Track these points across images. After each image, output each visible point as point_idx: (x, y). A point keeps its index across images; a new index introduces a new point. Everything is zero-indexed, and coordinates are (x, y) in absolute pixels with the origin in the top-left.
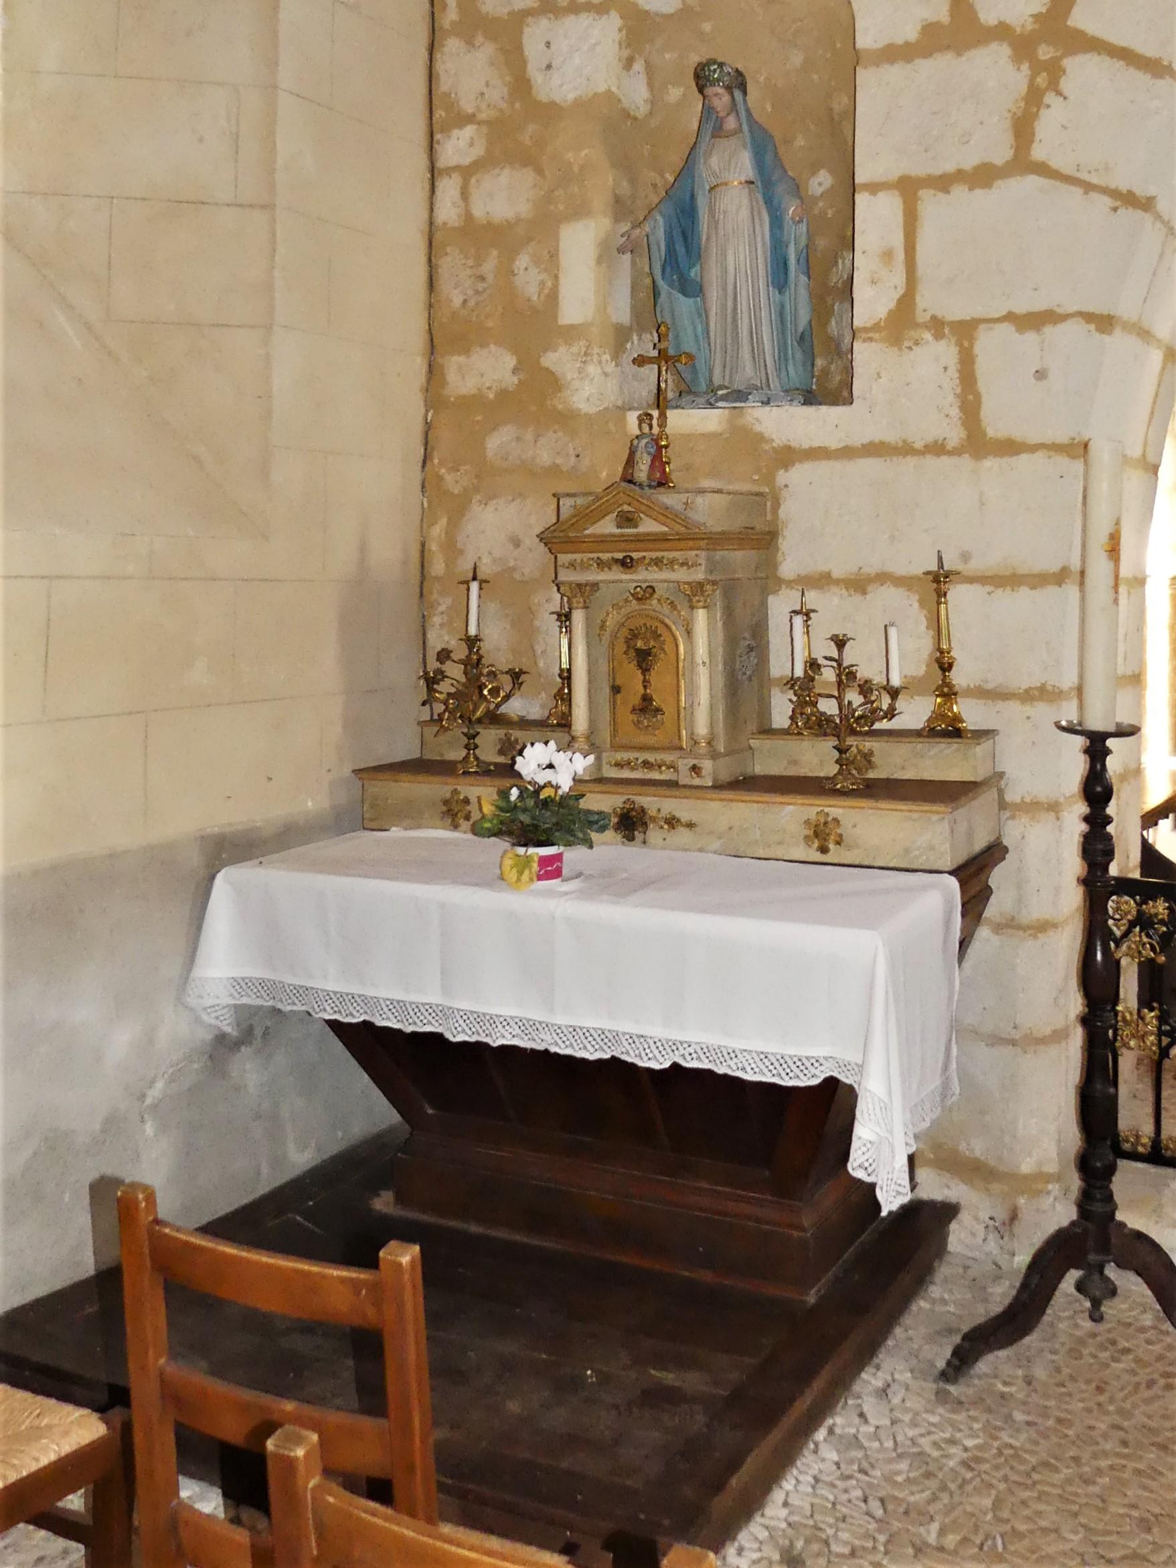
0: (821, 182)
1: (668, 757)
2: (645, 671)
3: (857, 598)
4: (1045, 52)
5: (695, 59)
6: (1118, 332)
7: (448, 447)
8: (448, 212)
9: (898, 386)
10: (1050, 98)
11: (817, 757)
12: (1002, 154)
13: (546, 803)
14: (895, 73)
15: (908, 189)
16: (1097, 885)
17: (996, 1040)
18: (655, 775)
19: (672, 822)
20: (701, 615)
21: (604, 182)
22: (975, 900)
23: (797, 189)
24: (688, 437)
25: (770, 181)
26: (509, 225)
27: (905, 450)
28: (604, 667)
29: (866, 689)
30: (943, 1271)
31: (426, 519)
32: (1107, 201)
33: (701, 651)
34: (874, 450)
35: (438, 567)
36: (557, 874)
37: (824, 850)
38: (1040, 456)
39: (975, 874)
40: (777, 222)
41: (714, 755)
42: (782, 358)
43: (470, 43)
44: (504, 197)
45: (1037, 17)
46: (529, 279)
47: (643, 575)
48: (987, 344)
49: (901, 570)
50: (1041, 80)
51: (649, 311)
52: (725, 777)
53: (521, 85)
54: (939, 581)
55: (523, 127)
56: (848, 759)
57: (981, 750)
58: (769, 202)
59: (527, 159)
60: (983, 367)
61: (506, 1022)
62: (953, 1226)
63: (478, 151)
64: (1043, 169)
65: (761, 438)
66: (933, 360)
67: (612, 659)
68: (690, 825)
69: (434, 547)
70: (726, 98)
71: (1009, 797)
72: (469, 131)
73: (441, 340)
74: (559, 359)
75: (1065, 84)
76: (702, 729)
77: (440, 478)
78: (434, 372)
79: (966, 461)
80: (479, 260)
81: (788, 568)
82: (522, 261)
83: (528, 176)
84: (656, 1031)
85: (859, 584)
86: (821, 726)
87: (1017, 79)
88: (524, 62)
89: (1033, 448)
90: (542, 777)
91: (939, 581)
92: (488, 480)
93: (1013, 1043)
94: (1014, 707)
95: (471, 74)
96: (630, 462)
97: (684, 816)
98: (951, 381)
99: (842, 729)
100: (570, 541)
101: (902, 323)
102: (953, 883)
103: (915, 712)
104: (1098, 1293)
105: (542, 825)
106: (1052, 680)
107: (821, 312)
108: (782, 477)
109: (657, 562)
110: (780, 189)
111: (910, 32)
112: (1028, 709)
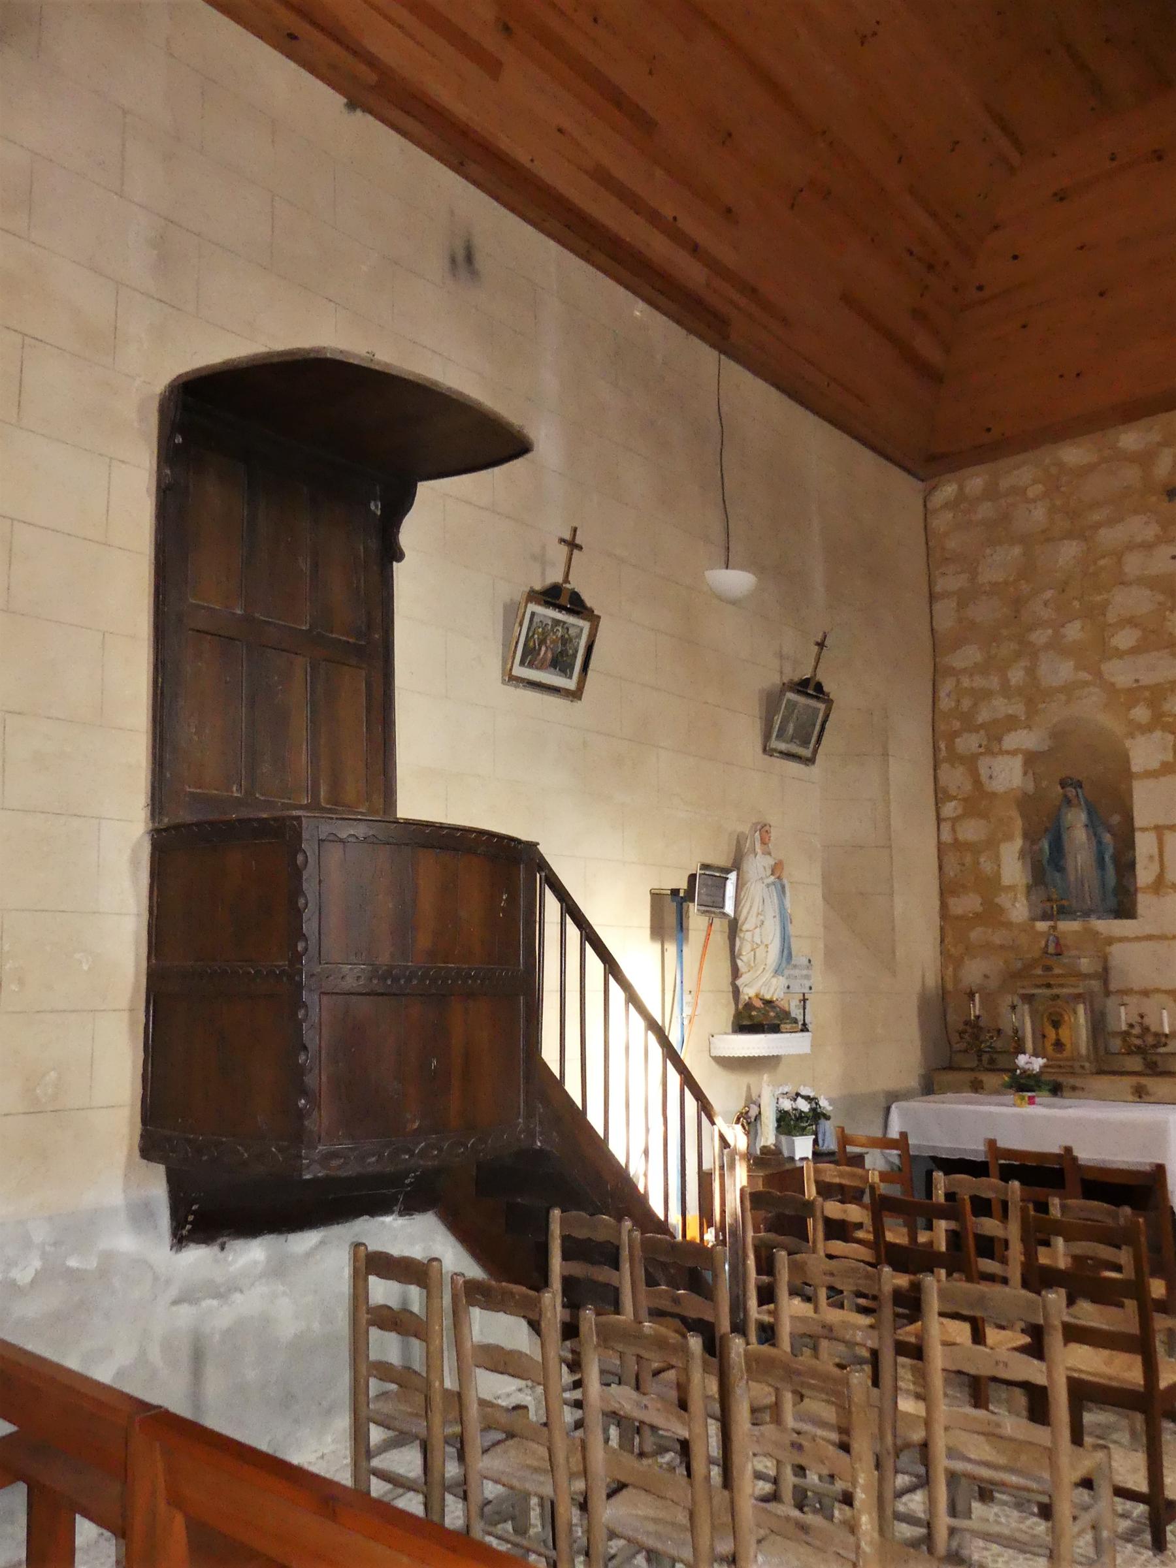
14: (1150, 783)
15: (1159, 830)
31: (944, 966)
34: (1150, 937)
36: (1033, 1103)
43: (953, 766)
44: (972, 831)
46: (987, 866)
47: (1056, 991)
53: (977, 783)
59: (983, 815)
63: (960, 811)
72: (953, 803)
73: (947, 890)
74: (1003, 900)
78: (944, 906)
83: (983, 822)
99: (1140, 1051)
101: (1159, 885)
110: (1100, 830)
111: (1155, 765)
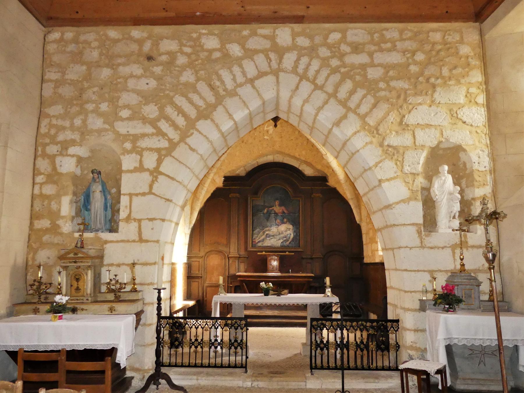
0: (114, 190)
1: (82, 298)
2: (78, 282)
3: (118, 268)
4: (155, 174)
5: (91, 170)
6: (166, 222)
7: (34, 239)
8: (37, 191)
9: (127, 230)
10: (155, 182)
11: (111, 297)
12: (147, 191)
13: (60, 306)
14: (129, 175)
15: (131, 195)
16: (160, 317)
17: (141, 346)
18: (79, 301)
19: (82, 310)
20: (89, 272)
21: (71, 189)
22: (138, 321)
23: (110, 193)
24: (87, 238)
25: (104, 191)
26: (50, 195)
27: (128, 241)
28: (69, 282)
29: (120, 284)
30: (131, 388)
31: (28, 253)
32: (164, 200)
33: (89, 278)
35: (30, 263)
37: (112, 312)
38: (152, 243)
39: (139, 315)
40: (106, 199)
41: (91, 297)
42: (105, 224)
43: (43, 159)
44: (49, 190)
45: (154, 168)
46: (54, 206)
47: (78, 264)
48: (143, 223)
49: (126, 263)
50: (154, 179)
51: (78, 213)
52: (93, 301)
53: (54, 168)
54: (134, 264)
55: (54, 177)
56: (116, 296)
57: (140, 294)
58: (104, 195)
59: (55, 183)
60: (142, 227)
61: (51, 345)
62: (133, 381)
63: (44, 180)
64: (154, 194)
65: (101, 239)
66: (134, 226)
67: (71, 280)
68: (86, 310)
69: (29, 259)
70: (97, 176)
71: (145, 302)
72: (42, 176)
73: (34, 216)
74: (60, 222)
75: (158, 180)
76: (89, 292)
77: (32, 245)
78: (31, 224)
79: (139, 244)
80: (43, 202)
81: (105, 263)
82: (53, 203)
83: (55, 186)
84: (81, 343)
85: (119, 265)
86: (112, 291)
87: (150, 178)
88: (55, 165)
89: (151, 241)
90: (59, 301)
91: (134, 264)
92: (43, 245)
93: (144, 346)
94: (146, 286)
95: (43, 165)
96: (77, 243)
97: (415, 212)
98: (137, 229)
100: (65, 258)
101: (128, 219)
102: (135, 316)
103: (128, 288)
104: (157, 384)
105: (58, 310)
106: (153, 282)
107: (113, 215)
108: (105, 246)
109: (82, 262)
110: (107, 193)
111: (132, 168)
112: (148, 287)
